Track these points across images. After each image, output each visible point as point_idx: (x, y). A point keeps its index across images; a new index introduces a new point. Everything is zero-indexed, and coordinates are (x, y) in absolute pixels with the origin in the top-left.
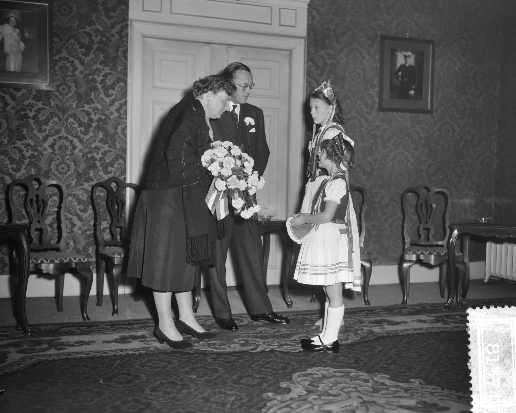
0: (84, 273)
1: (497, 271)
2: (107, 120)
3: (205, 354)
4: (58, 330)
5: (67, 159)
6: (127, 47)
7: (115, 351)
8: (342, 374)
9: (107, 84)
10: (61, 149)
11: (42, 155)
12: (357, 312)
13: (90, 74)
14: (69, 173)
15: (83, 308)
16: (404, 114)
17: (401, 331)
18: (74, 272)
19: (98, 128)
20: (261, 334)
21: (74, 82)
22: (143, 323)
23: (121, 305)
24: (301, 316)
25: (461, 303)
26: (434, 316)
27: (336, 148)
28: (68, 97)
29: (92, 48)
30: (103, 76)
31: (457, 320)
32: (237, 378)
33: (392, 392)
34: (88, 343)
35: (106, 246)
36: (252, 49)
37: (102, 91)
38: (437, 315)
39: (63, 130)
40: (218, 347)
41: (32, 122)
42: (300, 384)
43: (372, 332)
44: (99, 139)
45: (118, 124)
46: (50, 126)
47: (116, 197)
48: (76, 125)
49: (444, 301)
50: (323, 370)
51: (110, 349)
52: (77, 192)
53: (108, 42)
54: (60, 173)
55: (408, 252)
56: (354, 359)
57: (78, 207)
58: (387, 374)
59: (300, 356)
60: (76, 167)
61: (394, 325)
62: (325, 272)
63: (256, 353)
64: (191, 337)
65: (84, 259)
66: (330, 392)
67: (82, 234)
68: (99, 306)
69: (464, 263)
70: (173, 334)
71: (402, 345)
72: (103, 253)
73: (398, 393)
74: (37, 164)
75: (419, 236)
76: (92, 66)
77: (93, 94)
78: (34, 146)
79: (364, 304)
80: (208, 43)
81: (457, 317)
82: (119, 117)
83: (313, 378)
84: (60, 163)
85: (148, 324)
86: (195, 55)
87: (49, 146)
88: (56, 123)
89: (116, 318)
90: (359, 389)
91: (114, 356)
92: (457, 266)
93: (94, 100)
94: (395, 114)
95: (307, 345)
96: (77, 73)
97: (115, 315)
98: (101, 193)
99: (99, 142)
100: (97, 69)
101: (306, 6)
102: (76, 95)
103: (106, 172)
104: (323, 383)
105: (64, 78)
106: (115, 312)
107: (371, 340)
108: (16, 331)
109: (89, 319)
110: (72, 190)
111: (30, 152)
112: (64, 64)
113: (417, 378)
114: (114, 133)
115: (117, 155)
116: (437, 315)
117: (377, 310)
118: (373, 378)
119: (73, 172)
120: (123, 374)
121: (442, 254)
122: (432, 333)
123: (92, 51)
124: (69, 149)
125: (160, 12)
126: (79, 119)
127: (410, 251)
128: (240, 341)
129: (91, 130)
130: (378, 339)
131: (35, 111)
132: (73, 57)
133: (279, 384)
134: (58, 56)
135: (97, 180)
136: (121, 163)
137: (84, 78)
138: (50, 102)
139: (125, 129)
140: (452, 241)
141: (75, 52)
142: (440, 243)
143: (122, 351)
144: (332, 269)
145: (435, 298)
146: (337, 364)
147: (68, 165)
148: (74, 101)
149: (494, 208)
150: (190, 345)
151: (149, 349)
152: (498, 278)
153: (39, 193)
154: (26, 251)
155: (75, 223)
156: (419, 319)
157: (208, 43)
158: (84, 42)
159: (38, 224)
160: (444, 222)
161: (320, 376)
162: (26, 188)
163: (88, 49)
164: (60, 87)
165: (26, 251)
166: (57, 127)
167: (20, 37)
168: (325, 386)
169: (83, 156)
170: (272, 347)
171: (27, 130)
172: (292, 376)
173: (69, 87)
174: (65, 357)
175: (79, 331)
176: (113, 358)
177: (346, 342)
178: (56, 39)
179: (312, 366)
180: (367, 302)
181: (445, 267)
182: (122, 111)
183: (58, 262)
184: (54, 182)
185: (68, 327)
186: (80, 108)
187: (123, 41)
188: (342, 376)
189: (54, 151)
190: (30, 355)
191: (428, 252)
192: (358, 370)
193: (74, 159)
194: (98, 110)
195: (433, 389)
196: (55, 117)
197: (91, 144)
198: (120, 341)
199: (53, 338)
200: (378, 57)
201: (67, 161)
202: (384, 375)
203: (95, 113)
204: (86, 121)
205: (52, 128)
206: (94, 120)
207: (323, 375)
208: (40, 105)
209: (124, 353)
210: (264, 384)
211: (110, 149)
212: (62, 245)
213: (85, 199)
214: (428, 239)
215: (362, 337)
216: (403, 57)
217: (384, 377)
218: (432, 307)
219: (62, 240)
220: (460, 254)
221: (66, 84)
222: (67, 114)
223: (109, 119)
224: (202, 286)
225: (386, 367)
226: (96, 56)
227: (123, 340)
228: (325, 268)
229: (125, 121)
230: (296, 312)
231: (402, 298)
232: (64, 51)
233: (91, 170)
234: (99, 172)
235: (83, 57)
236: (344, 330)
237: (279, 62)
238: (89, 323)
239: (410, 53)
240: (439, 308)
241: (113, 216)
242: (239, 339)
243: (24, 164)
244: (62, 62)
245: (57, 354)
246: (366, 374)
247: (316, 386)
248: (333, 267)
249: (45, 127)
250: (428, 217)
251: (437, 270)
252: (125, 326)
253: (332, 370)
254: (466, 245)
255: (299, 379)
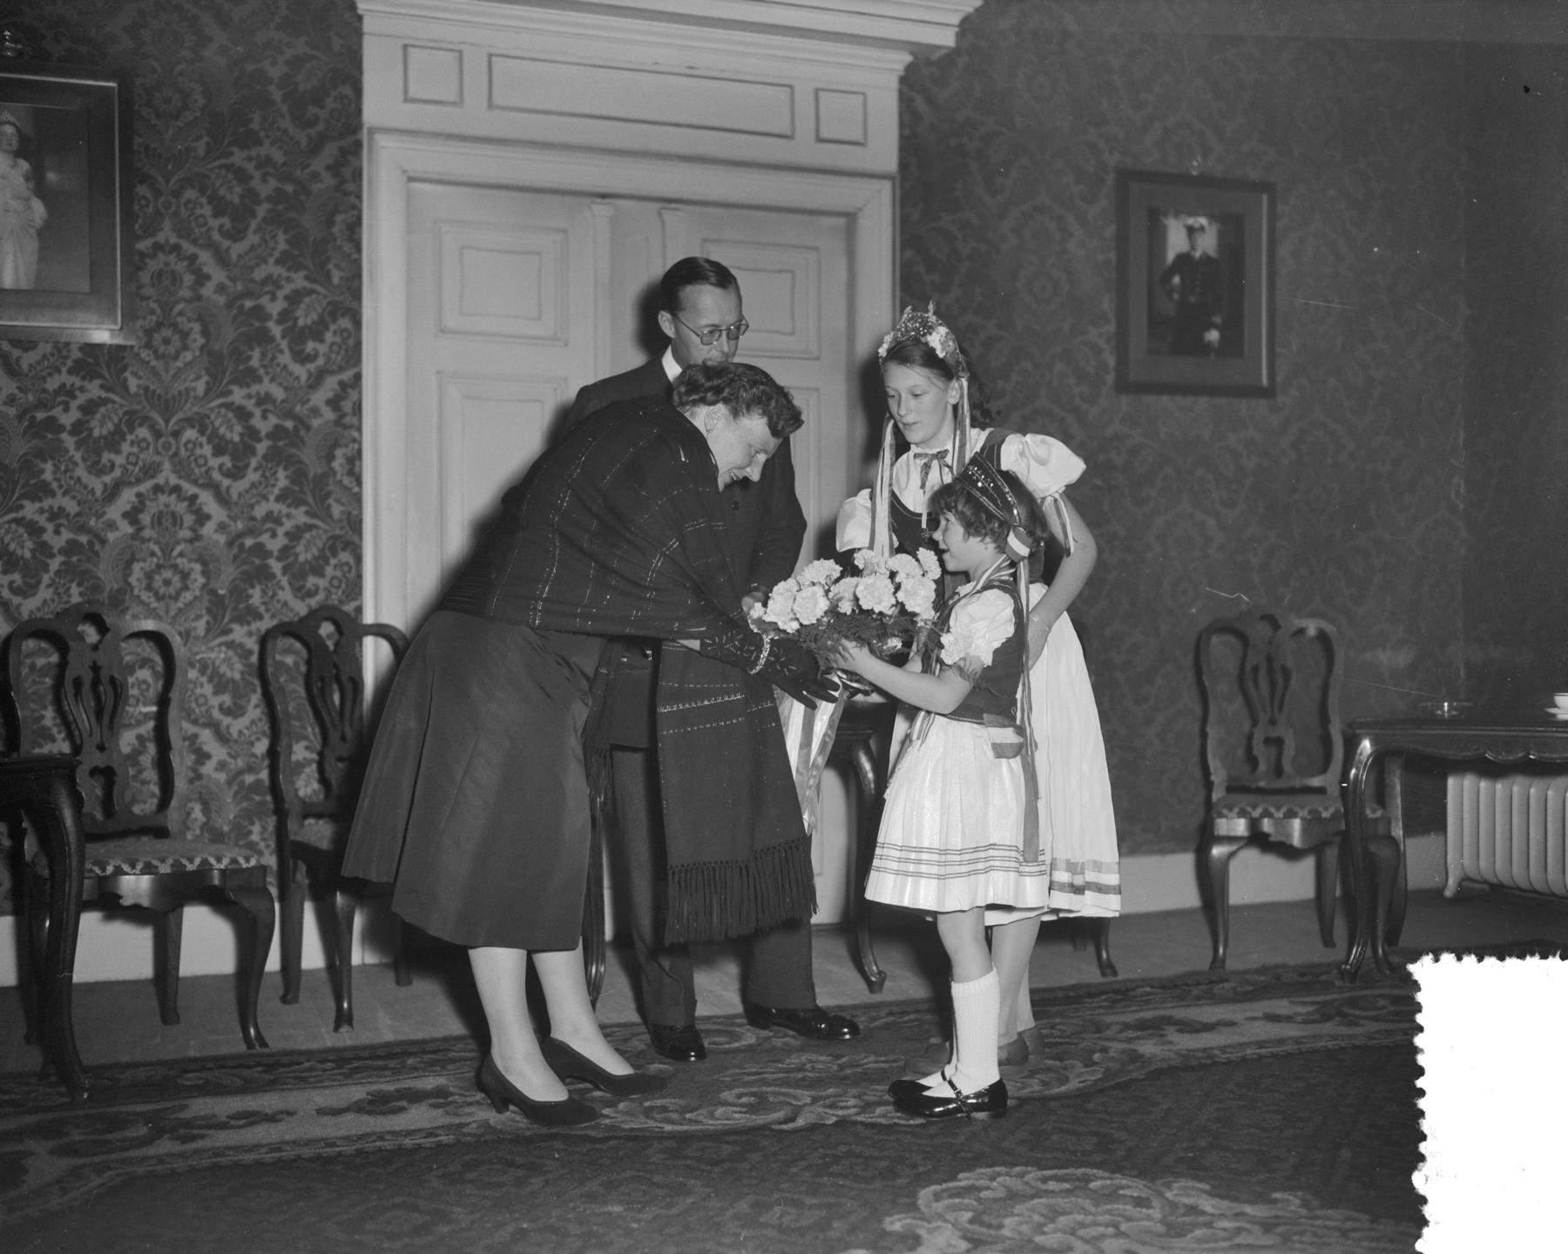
0: (247, 902)
1: (1483, 864)
2: (302, 433)
3: (639, 1139)
4: (174, 1080)
5: (181, 555)
6: (360, 211)
7: (361, 1137)
8: (1067, 1186)
9: (301, 322)
10: (160, 523)
11: (103, 542)
12: (1080, 997)
13: (248, 294)
14: (187, 596)
15: (246, 1010)
16: (1190, 400)
17: (1223, 1049)
18: (217, 900)
19: (274, 456)
20: (800, 1075)
21: (200, 319)
22: (434, 1052)
23: (359, 997)
24: (913, 1016)
25: (1388, 963)
26: (1313, 1003)
27: (984, 500)
28: (179, 364)
29: (253, 214)
30: (286, 298)
31: (1384, 1012)
32: (748, 1211)
33: (1225, 1235)
34: (272, 1118)
35: (305, 817)
36: (736, 211)
37: (284, 345)
38: (1320, 998)
39: (167, 466)
40: (675, 1116)
41: (69, 441)
42: (946, 1221)
43: (1135, 1057)
44: (276, 491)
45: (336, 445)
46: (125, 454)
47: (336, 666)
48: (207, 450)
49: (1337, 954)
50: (1007, 1174)
51: (341, 1133)
52: (213, 655)
53: (303, 198)
54: (159, 598)
55: (1225, 812)
56: (1095, 1140)
57: (215, 701)
58: (1200, 1181)
59: (932, 1137)
60: (208, 578)
61: (1197, 1031)
62: (943, 871)
63: (795, 1131)
64: (590, 1091)
65: (247, 860)
66: (1038, 1239)
67: (229, 783)
68: (290, 1003)
69: (1393, 841)
70: (536, 1082)
71: (1231, 1092)
72: (299, 838)
73: (1244, 1234)
74: (88, 571)
75: (1253, 762)
76: (252, 269)
77: (256, 354)
78: (78, 514)
79: (1098, 972)
80: (603, 196)
81: (1381, 1002)
82: (338, 423)
83: (979, 1200)
84: (159, 567)
85: (451, 1055)
86: (564, 231)
87: (125, 515)
88: (143, 445)
89: (346, 1038)
90: (1123, 1227)
91: (359, 1153)
92: (1373, 848)
93: (262, 371)
94: (1165, 400)
95: (910, 1098)
96: (208, 290)
97: (344, 1029)
98: (290, 656)
99: (278, 499)
100: (269, 279)
101: (894, 83)
102: (206, 358)
103: (302, 593)
104: (1013, 1215)
105: (167, 308)
106: (343, 1019)
107: (1136, 1080)
108: (41, 1089)
109: (264, 1044)
110: (195, 650)
111: (66, 535)
112: (167, 264)
113: (1291, 1189)
114: (319, 468)
115: (334, 538)
116: (1320, 998)
117: (1139, 991)
118: (1160, 1195)
119: (198, 593)
120: (395, 1206)
121: (1325, 815)
122: (1315, 1051)
123: (253, 225)
124: (186, 524)
125: (459, 102)
126: (215, 430)
127: (1230, 809)
128: (740, 1096)
129: (254, 463)
130: (1156, 1074)
131: (81, 408)
132: (195, 242)
133: (880, 1221)
134: (149, 242)
135: (273, 616)
136: (347, 564)
137: (229, 305)
138: (126, 379)
139: (355, 458)
140: (1356, 776)
141: (199, 226)
142: (1316, 782)
143: (381, 1138)
144: (961, 863)
145: (1304, 950)
146: (1048, 1155)
147: (182, 572)
148: (198, 378)
149: (1462, 673)
150: (592, 1115)
151: (465, 1130)
152: (1486, 882)
153: (101, 658)
154: (72, 838)
155: (206, 748)
156: (1268, 1011)
157: (603, 196)
158: (228, 197)
159: (98, 754)
160: (1324, 720)
161: (1001, 1193)
162: (60, 644)
163: (240, 217)
164: (156, 335)
165: (72, 838)
166: (148, 456)
167: (31, 185)
168: (1020, 1224)
169: (230, 544)
170: (840, 1113)
171: (57, 467)
172: (914, 1195)
173: (184, 335)
174: (206, 1162)
175: (239, 1082)
176: (358, 1161)
177: (1063, 1088)
178: (142, 190)
179: (971, 1164)
180: (1107, 967)
181: (1332, 853)
182: (347, 406)
183: (168, 870)
184: (149, 625)
185: (202, 1069)
186: (218, 397)
187: (347, 194)
188: (1068, 1192)
189: (140, 529)
190: (96, 1159)
191: (1283, 810)
192: (1113, 1172)
193: (201, 555)
194: (274, 401)
195: (1347, 1219)
196: (141, 425)
197: (252, 507)
198: (369, 1108)
199: (159, 1107)
200: (1110, 231)
201: (179, 560)
202: (1191, 1183)
203: (265, 412)
204: (236, 438)
205: (132, 459)
206: (263, 434)
207: (1008, 1189)
208: (94, 390)
209: (387, 1145)
210: (835, 1224)
211: (310, 521)
212: (173, 818)
213: (237, 676)
214: (1278, 771)
215: (1108, 1073)
216: (1183, 233)
217: (1193, 1188)
218: (1302, 975)
219: (174, 803)
220: (1379, 814)
221: (175, 326)
222: (180, 415)
223: (308, 428)
224: (608, 933)
225: (1193, 1159)
226: (263, 239)
227: (379, 1104)
228: (943, 858)
229: (356, 434)
230: (898, 1003)
231: (1210, 953)
232: (167, 225)
233: (253, 587)
234: (280, 592)
235: (226, 243)
236: (1014, 1056)
237: (816, 249)
238: (270, 1055)
239: (1203, 221)
240: (1323, 978)
241: (328, 724)
242: (737, 1090)
243: (47, 571)
244: (162, 257)
245: (182, 1155)
246: (1140, 1183)
247: (994, 1222)
248: (967, 857)
249: (112, 456)
250: (1276, 703)
251: (1308, 865)
252: (380, 1063)
253: (1033, 1175)
254: (1393, 787)
255: (939, 1206)
